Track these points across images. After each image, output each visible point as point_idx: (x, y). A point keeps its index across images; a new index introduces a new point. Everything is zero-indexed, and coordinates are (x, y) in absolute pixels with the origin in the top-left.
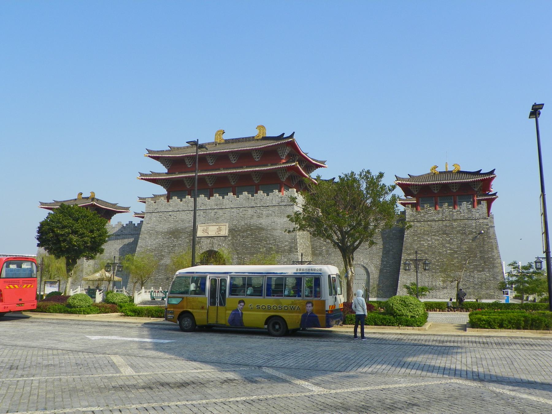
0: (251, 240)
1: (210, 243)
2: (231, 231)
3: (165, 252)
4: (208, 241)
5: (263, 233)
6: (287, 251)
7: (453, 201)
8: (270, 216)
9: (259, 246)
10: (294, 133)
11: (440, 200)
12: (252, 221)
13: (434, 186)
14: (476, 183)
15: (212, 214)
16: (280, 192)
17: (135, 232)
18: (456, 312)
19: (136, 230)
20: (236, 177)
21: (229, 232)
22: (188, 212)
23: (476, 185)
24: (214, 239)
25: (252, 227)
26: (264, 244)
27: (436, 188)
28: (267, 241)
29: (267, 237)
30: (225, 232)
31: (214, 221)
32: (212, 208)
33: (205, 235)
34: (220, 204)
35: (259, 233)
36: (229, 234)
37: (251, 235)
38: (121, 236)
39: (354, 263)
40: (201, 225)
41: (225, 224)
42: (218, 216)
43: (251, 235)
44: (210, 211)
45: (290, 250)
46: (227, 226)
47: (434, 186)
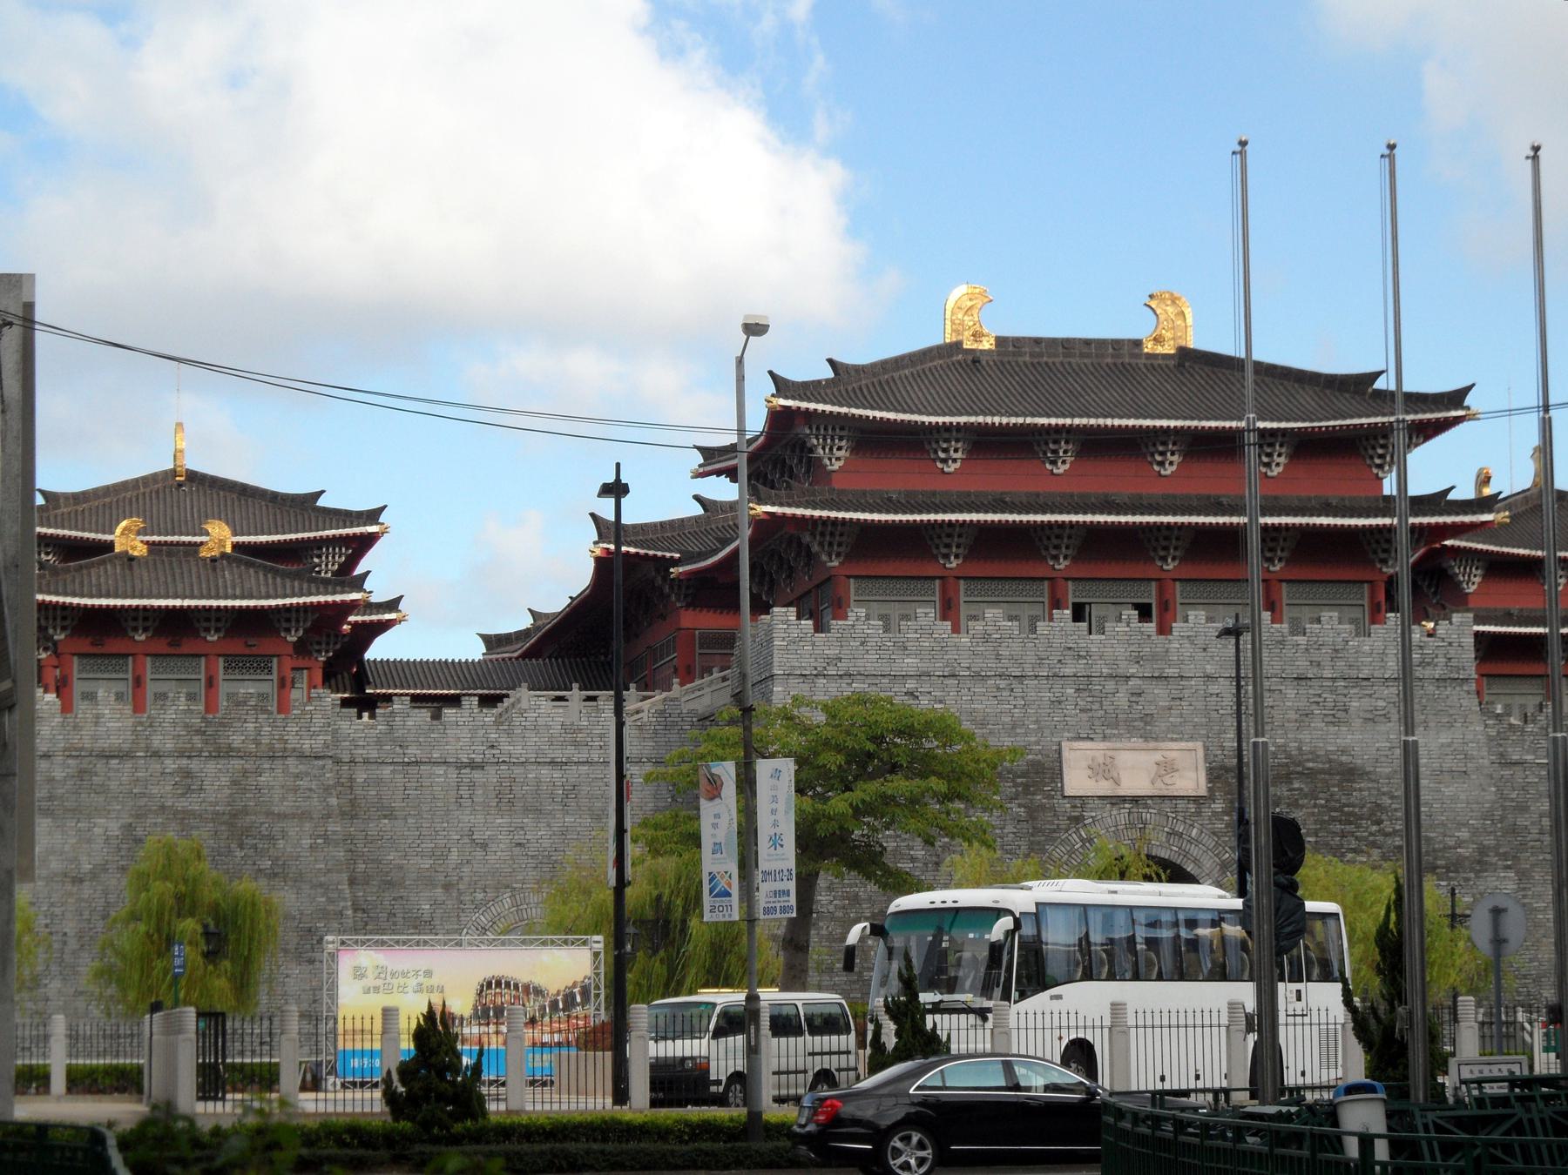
0: (1313, 814)
1: (1130, 826)
2: (1218, 777)
3: (913, 859)
4: (1122, 815)
5: (1361, 790)
6: (1467, 863)
7: (130, 676)
8: (1382, 719)
9: (1352, 840)
10: (771, 373)
11: (80, 672)
12: (1305, 736)
13: (288, 615)
14: (294, 615)
15: (1122, 699)
16: (1079, 621)
17: (570, 750)
18: (779, 1120)
19: (575, 743)
20: (828, 533)
21: (1210, 780)
22: (1003, 683)
23: (293, 624)
24: (1147, 806)
25: (1308, 760)
26: (1371, 834)
27: (140, 621)
28: (1382, 822)
29: (1378, 805)
30: (1191, 780)
31: (1132, 731)
32: (1120, 671)
33: (1104, 788)
34: (1154, 658)
35: (1342, 789)
36: (1210, 789)
37: (1313, 795)
38: (491, 770)
39: (142, 928)
40: (1077, 745)
41: (1190, 745)
42: (1151, 709)
43: (1313, 795)
44: (1110, 685)
45: (1479, 862)
46: (1201, 753)
47: (288, 615)
